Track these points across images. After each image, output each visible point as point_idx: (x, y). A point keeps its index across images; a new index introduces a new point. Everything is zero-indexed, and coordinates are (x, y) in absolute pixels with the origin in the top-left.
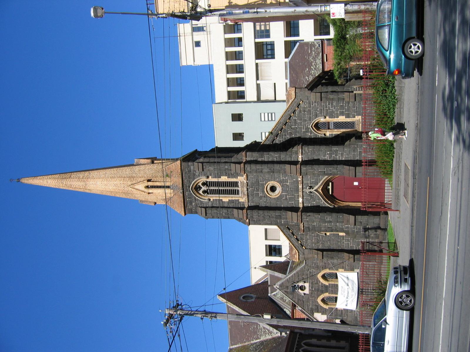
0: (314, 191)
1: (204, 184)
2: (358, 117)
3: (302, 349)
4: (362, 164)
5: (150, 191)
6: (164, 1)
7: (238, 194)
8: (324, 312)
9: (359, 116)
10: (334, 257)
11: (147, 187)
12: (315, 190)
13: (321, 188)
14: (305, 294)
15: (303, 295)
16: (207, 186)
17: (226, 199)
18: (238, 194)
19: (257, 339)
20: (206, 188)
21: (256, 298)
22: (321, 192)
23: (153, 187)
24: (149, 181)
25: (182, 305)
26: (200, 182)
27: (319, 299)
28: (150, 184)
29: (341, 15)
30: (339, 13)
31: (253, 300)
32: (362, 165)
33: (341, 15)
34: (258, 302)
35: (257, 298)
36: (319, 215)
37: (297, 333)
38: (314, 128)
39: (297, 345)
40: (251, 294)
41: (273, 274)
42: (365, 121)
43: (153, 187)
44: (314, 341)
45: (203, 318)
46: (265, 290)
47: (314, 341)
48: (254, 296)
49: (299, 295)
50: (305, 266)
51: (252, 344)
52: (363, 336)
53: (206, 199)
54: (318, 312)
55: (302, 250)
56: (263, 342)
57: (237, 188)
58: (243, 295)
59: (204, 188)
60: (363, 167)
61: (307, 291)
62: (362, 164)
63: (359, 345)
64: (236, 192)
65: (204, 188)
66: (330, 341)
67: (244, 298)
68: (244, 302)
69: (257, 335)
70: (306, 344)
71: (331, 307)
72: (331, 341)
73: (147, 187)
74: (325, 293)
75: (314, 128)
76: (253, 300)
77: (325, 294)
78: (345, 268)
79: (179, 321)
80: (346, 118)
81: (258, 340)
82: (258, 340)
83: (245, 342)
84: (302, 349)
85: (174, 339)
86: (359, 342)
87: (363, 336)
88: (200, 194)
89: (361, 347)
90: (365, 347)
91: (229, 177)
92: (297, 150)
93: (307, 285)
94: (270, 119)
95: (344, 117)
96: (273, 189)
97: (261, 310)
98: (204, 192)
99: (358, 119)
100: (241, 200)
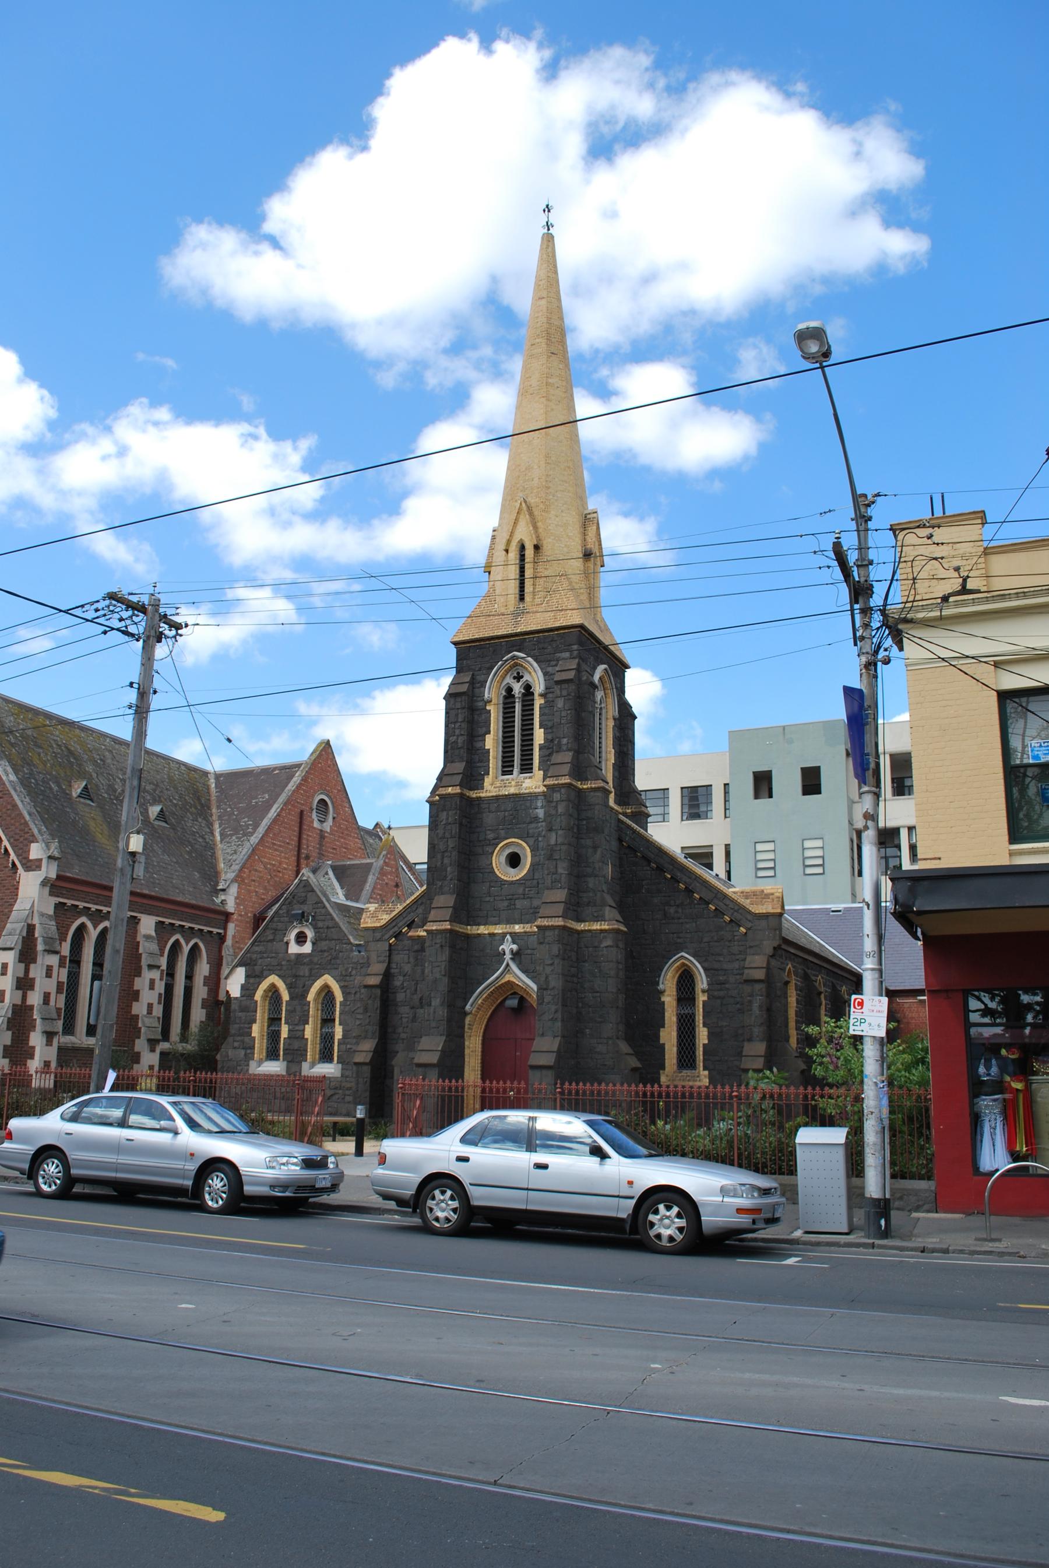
0: (505, 963)
1: (528, 687)
2: (705, 1076)
3: (182, 941)
4: (488, 1082)
5: (514, 555)
6: (876, 530)
7: (504, 773)
8: (248, 990)
9: (708, 1080)
10: (369, 1014)
11: (522, 548)
12: (508, 965)
13: (515, 981)
14: (287, 943)
15: (285, 940)
16: (524, 695)
17: (492, 742)
18: (503, 771)
19: (221, 835)
20: (517, 692)
21: (321, 831)
22: (503, 981)
23: (522, 558)
24: (537, 548)
25: (178, 637)
26: (532, 676)
27: (277, 978)
28: (529, 553)
29: (858, 1023)
30: (863, 1021)
31: (316, 824)
32: (483, 1079)
33: (858, 1023)
34: (310, 836)
35: (322, 834)
36: (445, 975)
37: (225, 929)
38: (678, 963)
39: (192, 929)
40: (334, 818)
41: (373, 871)
42: (310, 1081)
43: (522, 558)
44: (203, 969)
45: (132, 687)
46: (345, 852)
47: (203, 969)
48: (328, 826)
49: (285, 932)
50: (351, 943)
51: (210, 825)
52: (457, 1090)
53: (492, 693)
54: (247, 976)
55: (387, 936)
56: (213, 849)
57: (516, 770)
58: (327, 796)
59: (517, 688)
60: (479, 1082)
61: (294, 949)
62: (488, 1082)
63: (195, 1073)
64: (507, 767)
65: (517, 688)
66: (202, 1008)
67: (322, 801)
68: (311, 803)
69: (231, 835)
70: (195, 949)
71: (258, 1009)
72: (204, 1011)
73: (522, 548)
74: (290, 994)
75: (678, 963)
76: (316, 824)
77: (287, 991)
78: (344, 1043)
79: (124, 629)
80: (704, 1045)
81: (218, 838)
82: (218, 838)
83: (218, 807)
84: (182, 941)
85: (87, 620)
86: (209, 1073)
87: (457, 1090)
88: (503, 678)
89: (733, 1092)
90: (191, 1087)
91: (541, 747)
92: (607, 917)
93: (307, 948)
94: (820, 861)
95: (706, 1042)
96: (514, 860)
97: (288, 843)
98: (509, 690)
99: (702, 1077)
100: (488, 781)
